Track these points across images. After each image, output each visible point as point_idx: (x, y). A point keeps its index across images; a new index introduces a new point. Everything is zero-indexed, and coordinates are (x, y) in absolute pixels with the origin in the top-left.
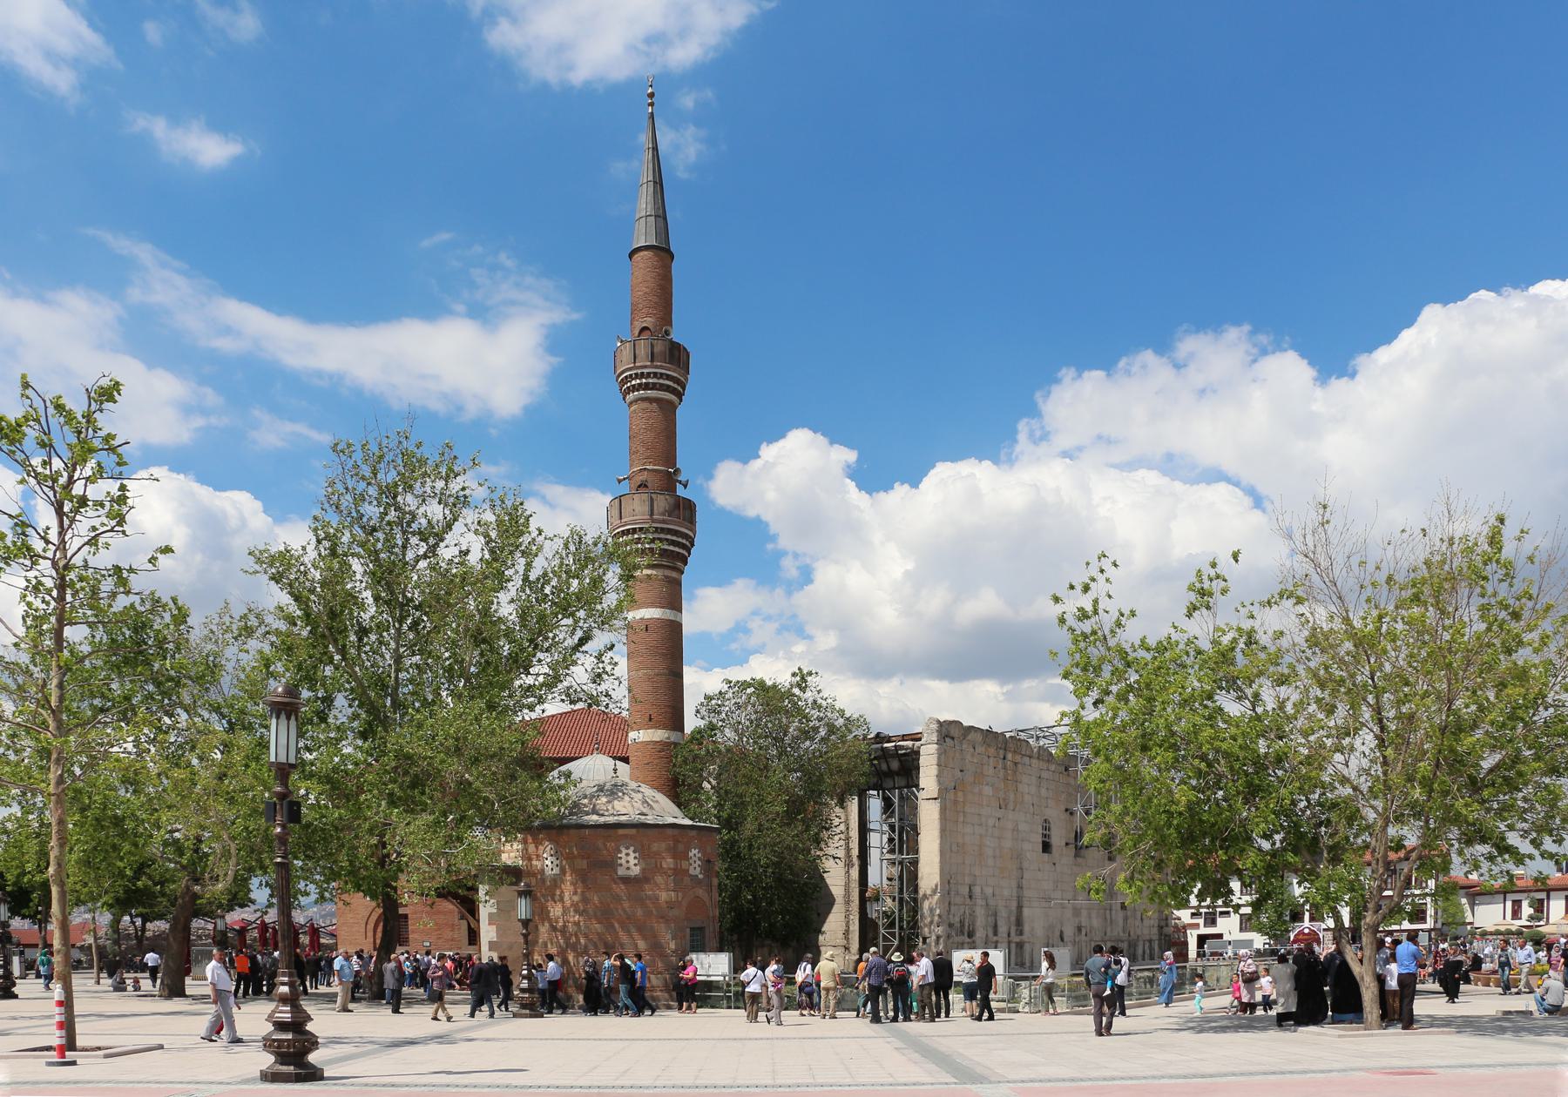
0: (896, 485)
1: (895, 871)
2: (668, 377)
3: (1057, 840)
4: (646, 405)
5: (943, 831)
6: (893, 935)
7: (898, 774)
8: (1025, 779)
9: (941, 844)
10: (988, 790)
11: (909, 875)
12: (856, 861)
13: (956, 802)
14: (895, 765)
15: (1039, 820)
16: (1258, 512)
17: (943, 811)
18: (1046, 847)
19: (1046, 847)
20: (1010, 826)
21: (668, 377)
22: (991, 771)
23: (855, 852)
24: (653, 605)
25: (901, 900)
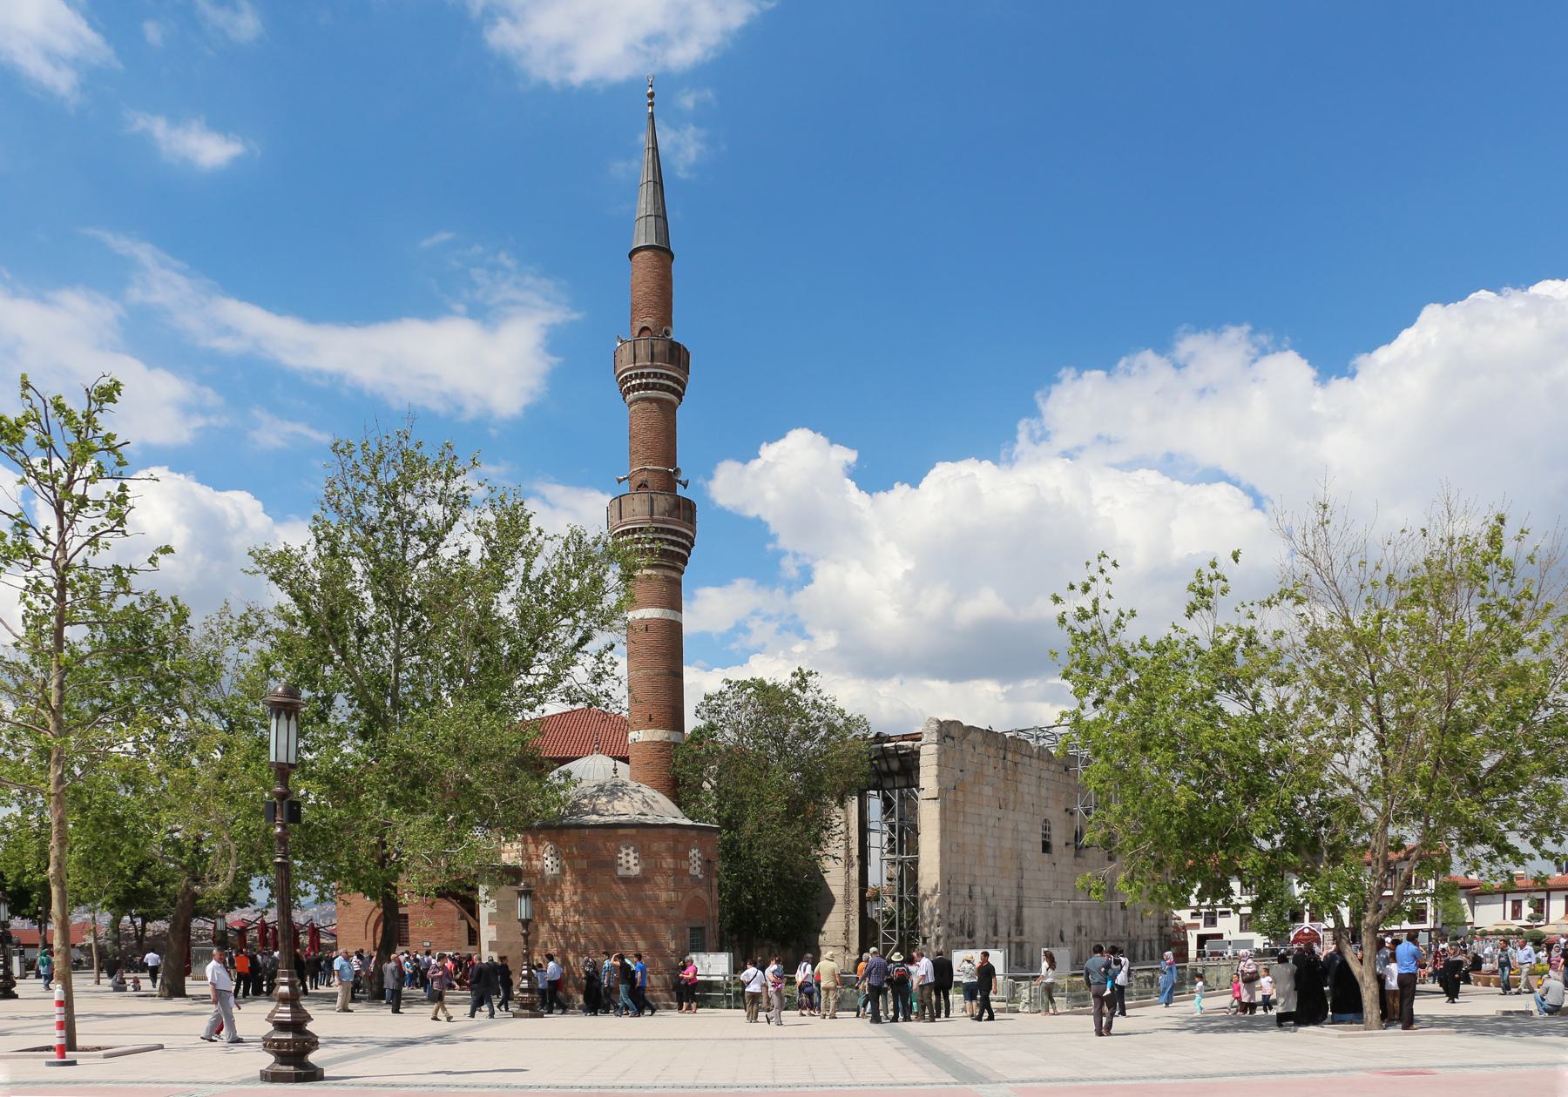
1: (895, 871)
2: (668, 377)
3: (1057, 840)
4: (646, 405)
5: (943, 831)
6: (893, 935)
7: (898, 774)
8: (1025, 779)
9: (941, 844)
10: (988, 790)
11: (909, 875)
12: (856, 861)
13: (956, 802)
14: (895, 765)
15: (1039, 820)
16: (1258, 512)
17: (943, 811)
18: (1046, 847)
19: (1046, 847)
20: (1010, 826)
21: (668, 377)
22: (991, 771)
23: (855, 852)
24: (653, 605)
25: (901, 900)
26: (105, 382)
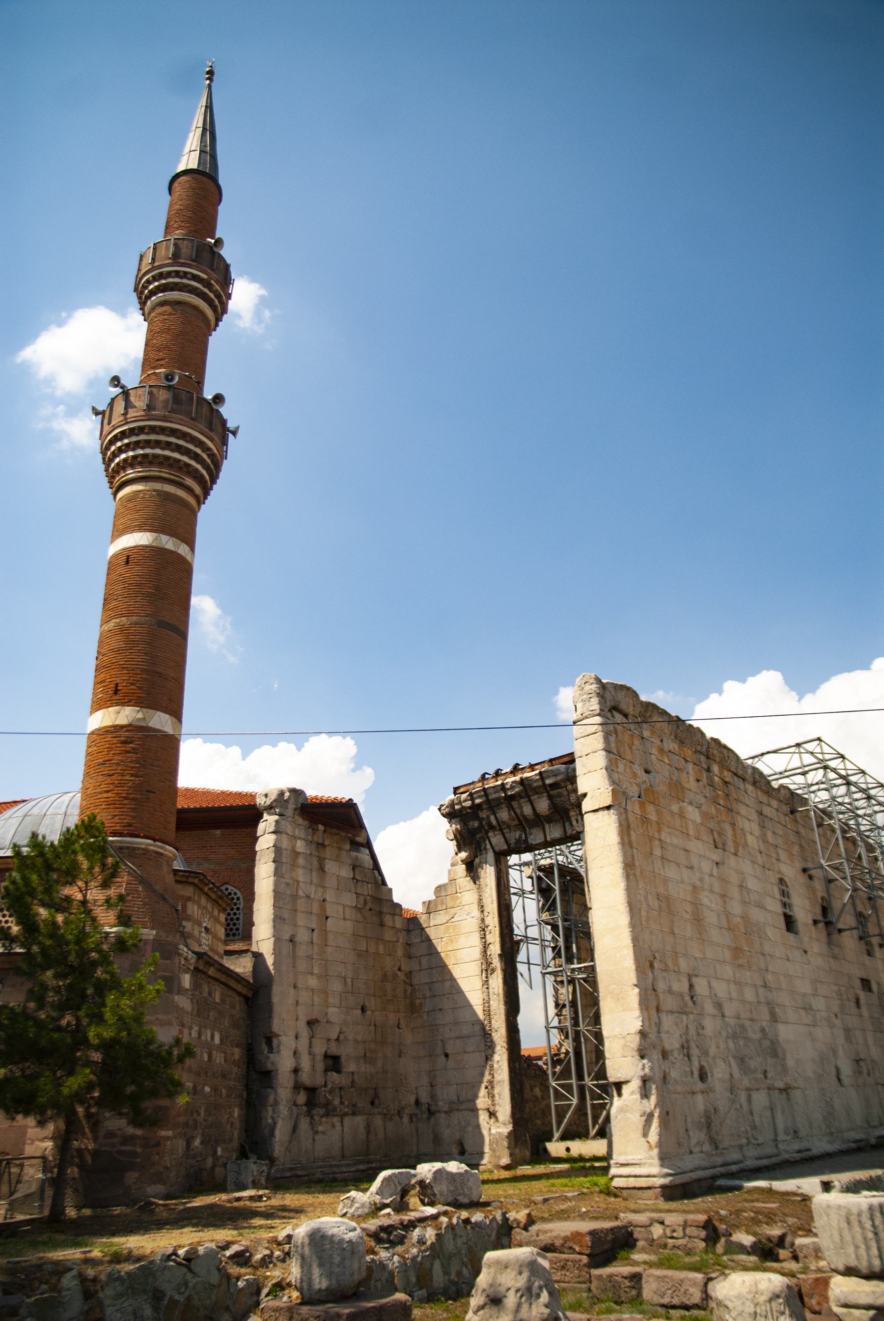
0: (562, 689)
1: (565, 993)
2: (195, 278)
3: (803, 913)
4: (160, 310)
5: (629, 867)
6: (568, 1088)
7: (549, 819)
8: (743, 810)
9: (629, 890)
10: (693, 814)
11: (582, 1006)
12: (497, 963)
13: (645, 820)
14: (543, 805)
15: (773, 878)
16: (791, 936)
17: (625, 830)
18: (790, 923)
19: (790, 923)
20: (734, 879)
21: (195, 278)
22: (692, 784)
23: (495, 949)
24: (141, 528)
25: (577, 1034)
26: (30, 835)
